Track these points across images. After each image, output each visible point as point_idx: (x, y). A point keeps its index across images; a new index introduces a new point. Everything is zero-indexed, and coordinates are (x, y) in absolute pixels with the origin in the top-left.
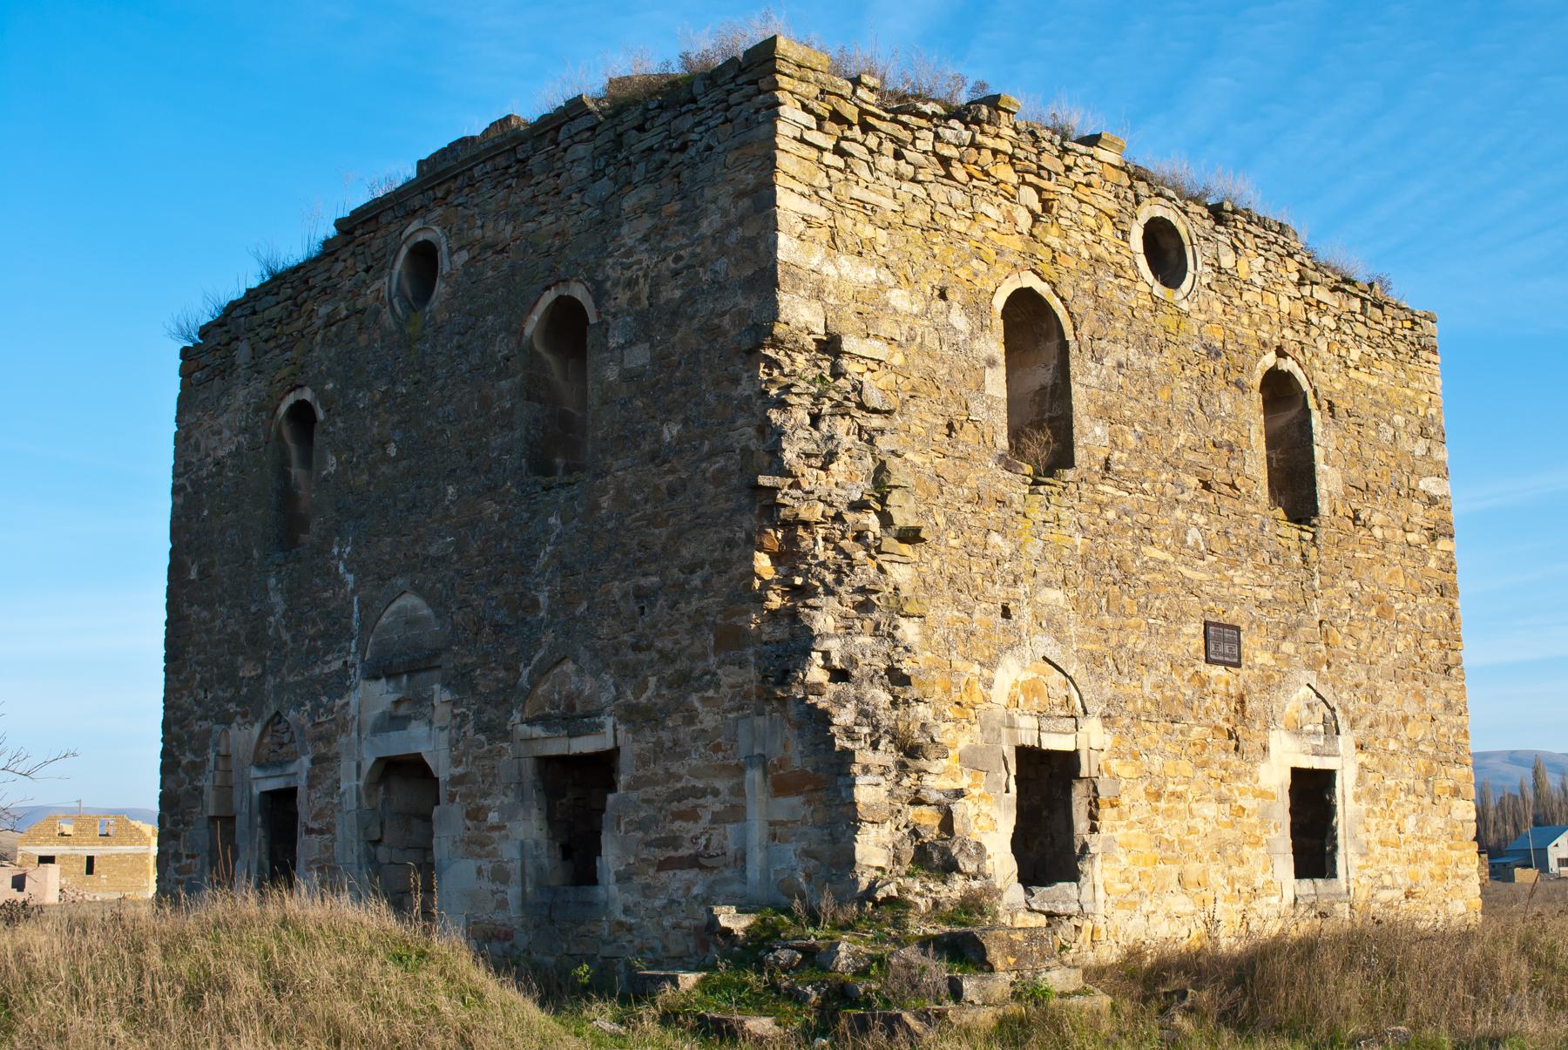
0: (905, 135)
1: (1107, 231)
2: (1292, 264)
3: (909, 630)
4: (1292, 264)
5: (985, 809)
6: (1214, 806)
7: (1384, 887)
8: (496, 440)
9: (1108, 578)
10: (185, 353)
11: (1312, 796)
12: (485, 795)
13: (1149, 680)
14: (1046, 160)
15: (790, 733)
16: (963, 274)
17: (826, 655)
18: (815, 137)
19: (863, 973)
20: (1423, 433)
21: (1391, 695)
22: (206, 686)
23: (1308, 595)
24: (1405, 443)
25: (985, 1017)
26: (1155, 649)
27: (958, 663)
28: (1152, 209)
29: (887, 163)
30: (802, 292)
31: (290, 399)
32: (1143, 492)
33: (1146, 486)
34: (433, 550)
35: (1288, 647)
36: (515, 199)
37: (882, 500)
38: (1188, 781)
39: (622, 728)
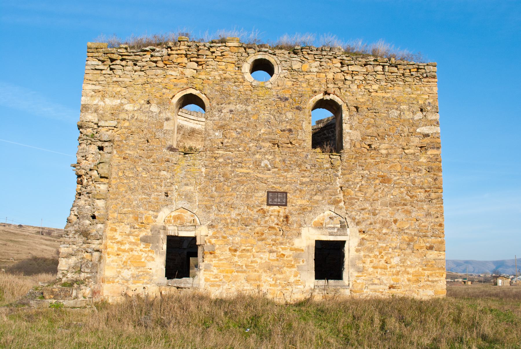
5: (150, 254)
6: (267, 254)
7: (373, 284)
30: (90, 111)
32: (239, 151)
33: (240, 149)
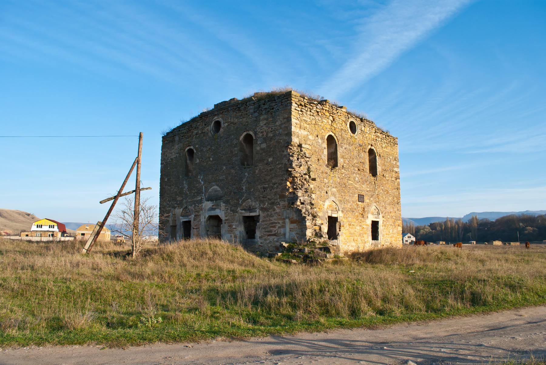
0: (311, 108)
1: (344, 124)
2: (374, 129)
3: (313, 196)
4: (374, 129)
8: (234, 159)
9: (343, 186)
10: (163, 137)
11: (375, 225)
12: (232, 223)
13: (349, 205)
14: (334, 111)
15: (294, 213)
16: (320, 132)
17: (300, 200)
18: (298, 109)
19: (310, 253)
20: (395, 160)
21: (388, 207)
22: (169, 201)
23: (375, 190)
24: (392, 162)
25: (330, 260)
26: (350, 199)
27: (319, 201)
28: (351, 120)
29: (309, 113)
31: (188, 148)
34: (220, 178)
35: (372, 199)
36: (238, 115)
37: (309, 173)
38: (355, 222)
39: (260, 212)
